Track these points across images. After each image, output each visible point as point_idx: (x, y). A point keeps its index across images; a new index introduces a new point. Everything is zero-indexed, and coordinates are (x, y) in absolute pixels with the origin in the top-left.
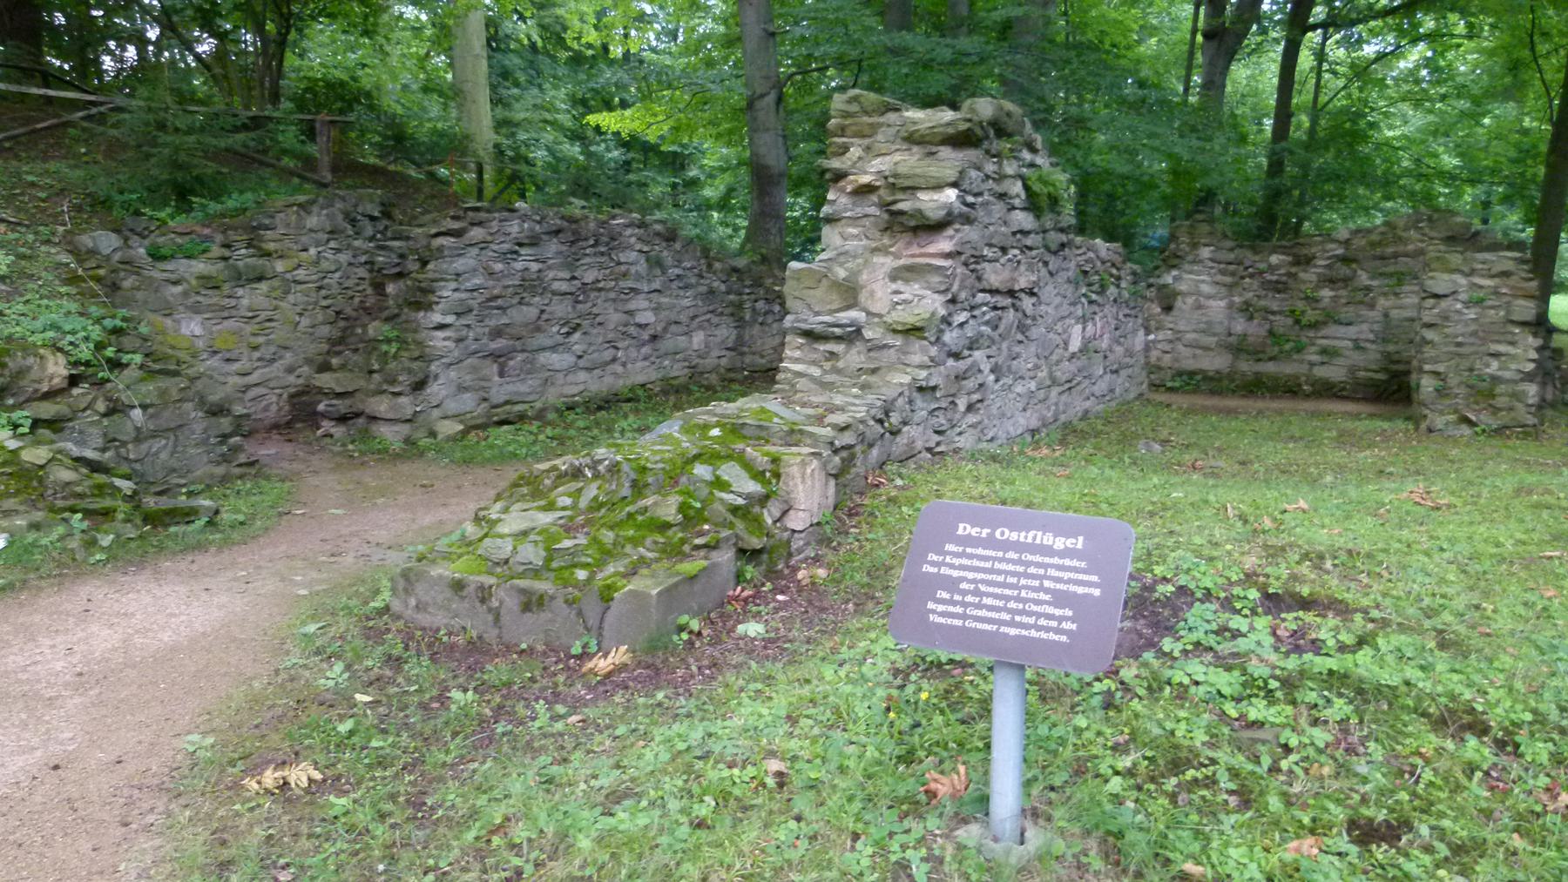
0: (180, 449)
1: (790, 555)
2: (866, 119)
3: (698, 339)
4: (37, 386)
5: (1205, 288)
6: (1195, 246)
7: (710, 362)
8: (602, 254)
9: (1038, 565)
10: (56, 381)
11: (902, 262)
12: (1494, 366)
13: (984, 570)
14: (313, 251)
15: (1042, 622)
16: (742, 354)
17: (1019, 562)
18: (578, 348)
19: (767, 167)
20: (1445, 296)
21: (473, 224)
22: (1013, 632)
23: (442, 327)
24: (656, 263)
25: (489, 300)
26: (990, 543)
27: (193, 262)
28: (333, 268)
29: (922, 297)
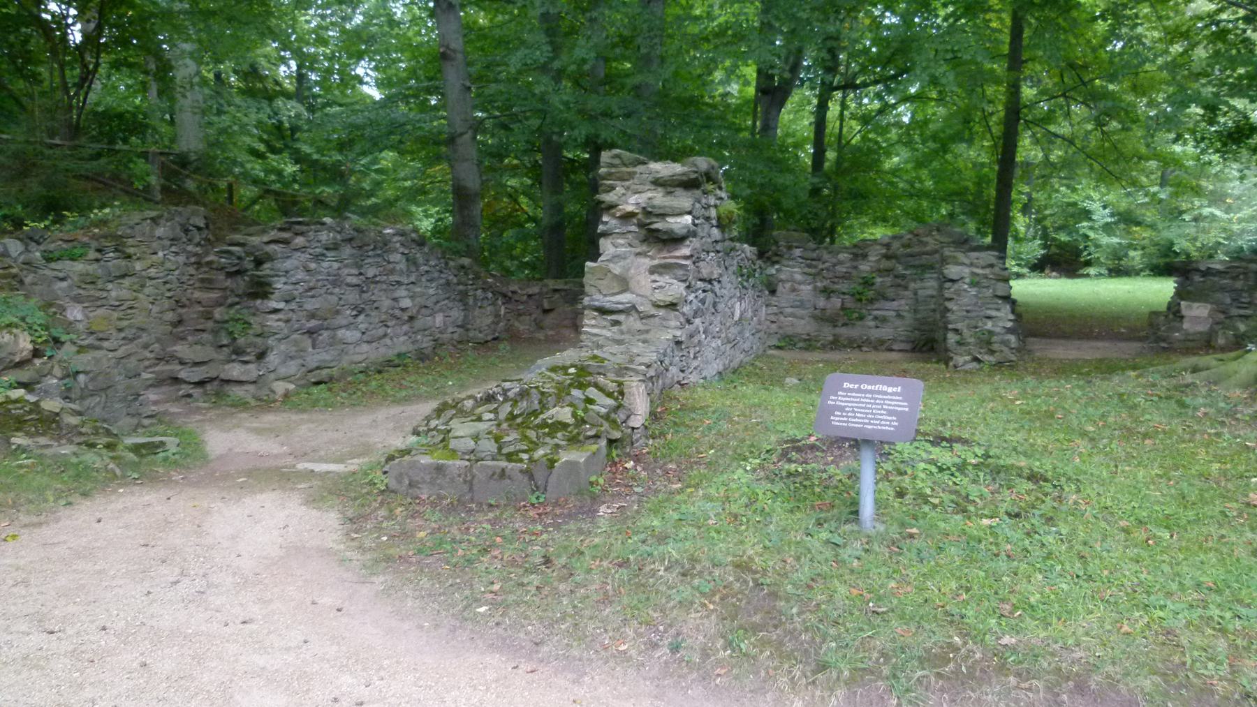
0: (109, 404)
1: (632, 444)
2: (624, 169)
3: (439, 319)
4: (12, 357)
5: (798, 277)
6: (790, 248)
7: (447, 336)
8: (379, 255)
9: (880, 399)
10: (25, 353)
11: (656, 262)
12: (989, 325)
13: (856, 402)
14: (161, 254)
15: (883, 422)
16: (468, 330)
17: (872, 398)
18: (362, 326)
19: (465, 188)
20: (957, 280)
21: (297, 234)
22: (870, 427)
23: (276, 311)
24: (412, 261)
25: (307, 291)
26: (859, 391)
27: (75, 263)
28: (174, 267)
29: (671, 284)
